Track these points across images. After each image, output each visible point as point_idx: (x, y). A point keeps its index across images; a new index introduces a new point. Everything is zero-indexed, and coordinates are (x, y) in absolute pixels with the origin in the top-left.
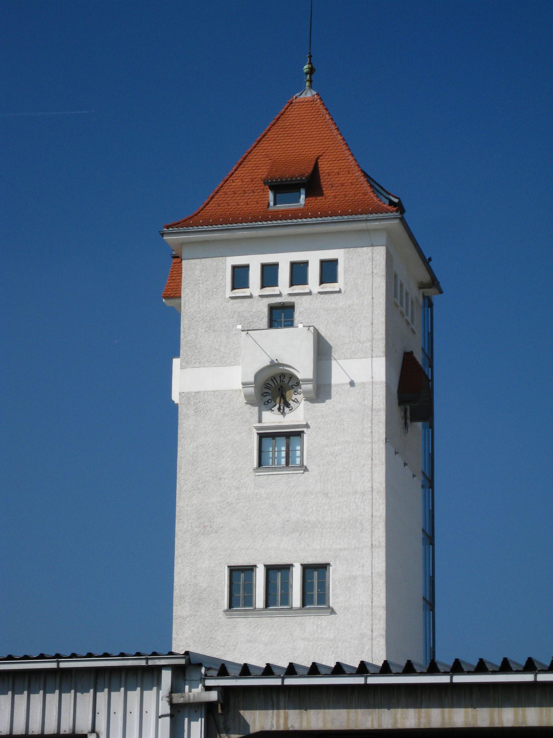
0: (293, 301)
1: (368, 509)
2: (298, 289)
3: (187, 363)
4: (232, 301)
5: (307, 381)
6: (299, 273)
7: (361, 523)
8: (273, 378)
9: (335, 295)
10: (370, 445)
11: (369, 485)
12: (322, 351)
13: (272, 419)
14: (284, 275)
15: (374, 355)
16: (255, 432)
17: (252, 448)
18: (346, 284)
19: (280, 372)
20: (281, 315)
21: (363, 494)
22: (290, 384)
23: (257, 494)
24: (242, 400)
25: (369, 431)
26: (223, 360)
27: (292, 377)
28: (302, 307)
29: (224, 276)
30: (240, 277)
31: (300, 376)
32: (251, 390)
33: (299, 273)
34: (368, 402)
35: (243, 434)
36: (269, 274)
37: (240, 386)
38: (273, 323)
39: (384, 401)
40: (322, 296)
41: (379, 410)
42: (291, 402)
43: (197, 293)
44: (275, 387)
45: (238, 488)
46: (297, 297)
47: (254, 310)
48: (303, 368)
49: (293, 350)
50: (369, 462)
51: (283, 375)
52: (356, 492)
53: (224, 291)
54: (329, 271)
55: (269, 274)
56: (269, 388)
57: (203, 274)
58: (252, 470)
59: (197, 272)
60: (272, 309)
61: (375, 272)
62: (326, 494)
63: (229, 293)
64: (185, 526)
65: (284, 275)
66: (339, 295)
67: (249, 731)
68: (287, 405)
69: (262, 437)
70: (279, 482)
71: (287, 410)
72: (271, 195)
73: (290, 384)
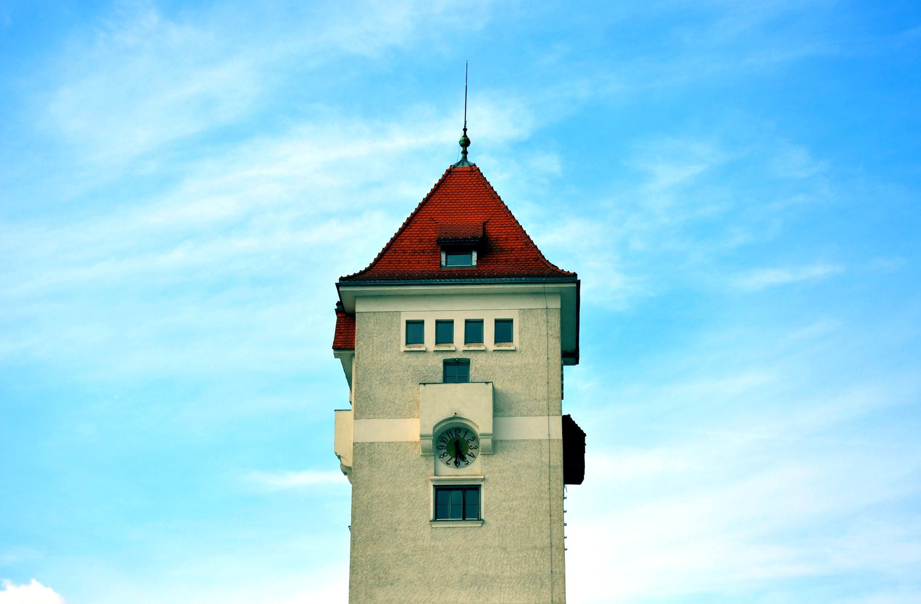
0: (468, 357)
1: (548, 565)
2: (473, 347)
3: (362, 414)
4: (406, 355)
5: (485, 435)
6: (474, 330)
7: (540, 579)
8: (448, 432)
9: (511, 354)
10: (548, 501)
11: (548, 541)
12: (500, 406)
13: (449, 473)
14: (459, 332)
15: (551, 413)
16: (431, 485)
17: (428, 501)
18: (521, 343)
19: (457, 426)
20: (456, 371)
21: (542, 549)
22: (466, 439)
23: (434, 547)
24: (418, 451)
25: (547, 487)
26: (399, 413)
27: (468, 431)
28: (478, 364)
29: (399, 330)
30: (415, 330)
31: (479, 431)
32: (429, 443)
33: (474, 330)
34: (545, 459)
35: (419, 486)
36: (444, 330)
37: (418, 438)
38: (447, 379)
39: (562, 458)
40: (498, 354)
41: (556, 467)
42: (467, 456)
43: (371, 346)
44: (454, 441)
45: (414, 540)
46: (473, 354)
47: (429, 365)
48: (480, 420)
49: (470, 403)
50: (548, 518)
51: (458, 429)
52: (535, 547)
53: (399, 345)
54: (504, 330)
55: (444, 330)
56: (444, 442)
57: (377, 328)
58: (428, 522)
59: (371, 326)
60: (446, 363)
61: (550, 333)
62: (505, 549)
63: (403, 348)
64: (359, 577)
65: (459, 332)
66: (514, 354)
67: (38, 580)
68: (463, 458)
69: (438, 489)
70: (457, 532)
71: (462, 463)
72: (443, 256)
73: (466, 439)
